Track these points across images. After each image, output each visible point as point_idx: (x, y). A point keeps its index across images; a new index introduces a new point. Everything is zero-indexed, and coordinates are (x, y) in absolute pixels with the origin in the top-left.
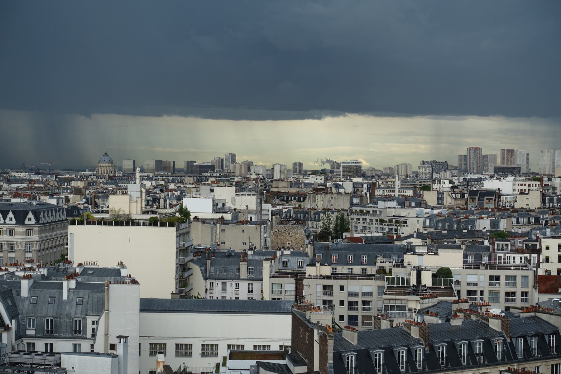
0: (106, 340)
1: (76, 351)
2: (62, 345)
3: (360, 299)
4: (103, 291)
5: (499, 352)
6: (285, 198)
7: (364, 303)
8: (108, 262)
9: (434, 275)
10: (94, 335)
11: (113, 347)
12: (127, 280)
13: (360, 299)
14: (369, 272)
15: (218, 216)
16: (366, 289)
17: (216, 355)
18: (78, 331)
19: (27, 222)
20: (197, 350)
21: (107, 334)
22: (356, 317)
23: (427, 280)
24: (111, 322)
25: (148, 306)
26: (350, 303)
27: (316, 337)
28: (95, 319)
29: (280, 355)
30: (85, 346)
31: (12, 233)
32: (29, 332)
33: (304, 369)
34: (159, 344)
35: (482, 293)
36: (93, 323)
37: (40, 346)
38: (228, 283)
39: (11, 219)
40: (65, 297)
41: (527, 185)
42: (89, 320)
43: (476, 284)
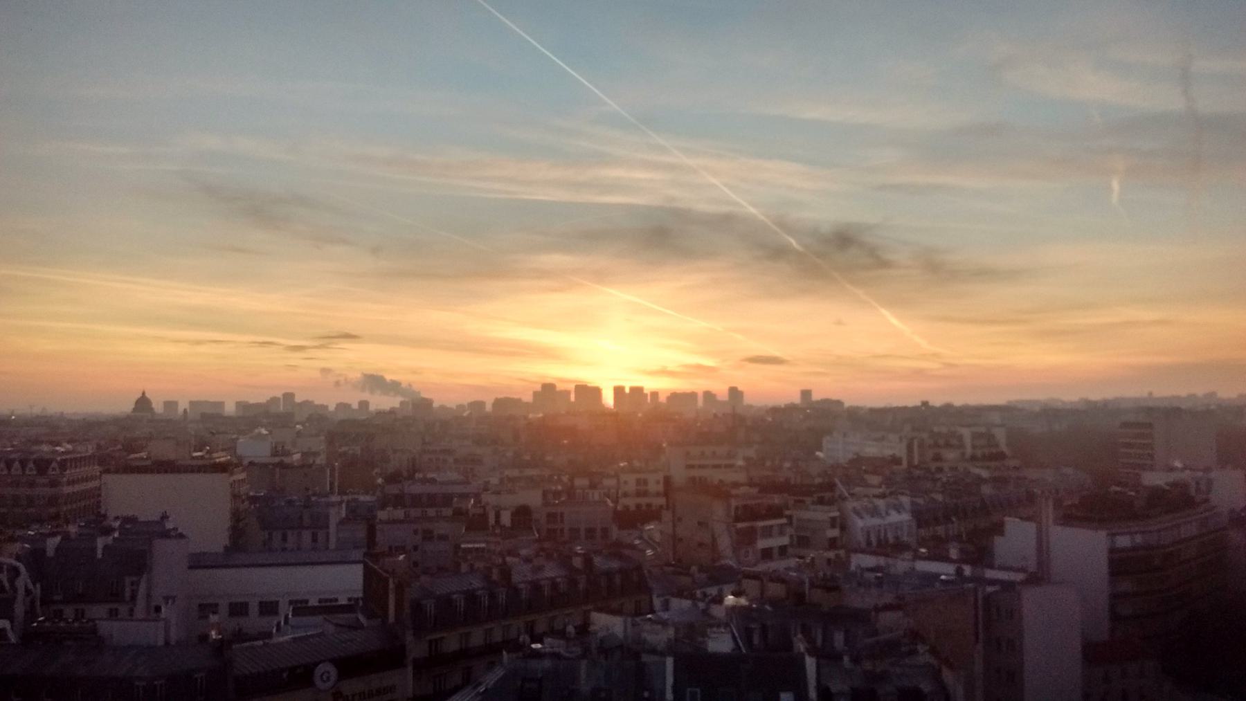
1: (113, 614)
2: (97, 611)
5: (487, 542)
8: (148, 513)
9: (512, 514)
10: (133, 597)
11: (158, 609)
12: (173, 533)
14: (444, 514)
15: (277, 460)
18: (115, 595)
19: (50, 472)
20: (254, 609)
21: (149, 596)
23: (506, 519)
25: (198, 562)
27: (391, 586)
28: (135, 579)
29: (349, 608)
30: (123, 609)
31: (32, 485)
32: (56, 598)
36: (132, 584)
37: (69, 612)
38: (289, 533)
39: (31, 470)
40: (99, 556)
42: (128, 580)
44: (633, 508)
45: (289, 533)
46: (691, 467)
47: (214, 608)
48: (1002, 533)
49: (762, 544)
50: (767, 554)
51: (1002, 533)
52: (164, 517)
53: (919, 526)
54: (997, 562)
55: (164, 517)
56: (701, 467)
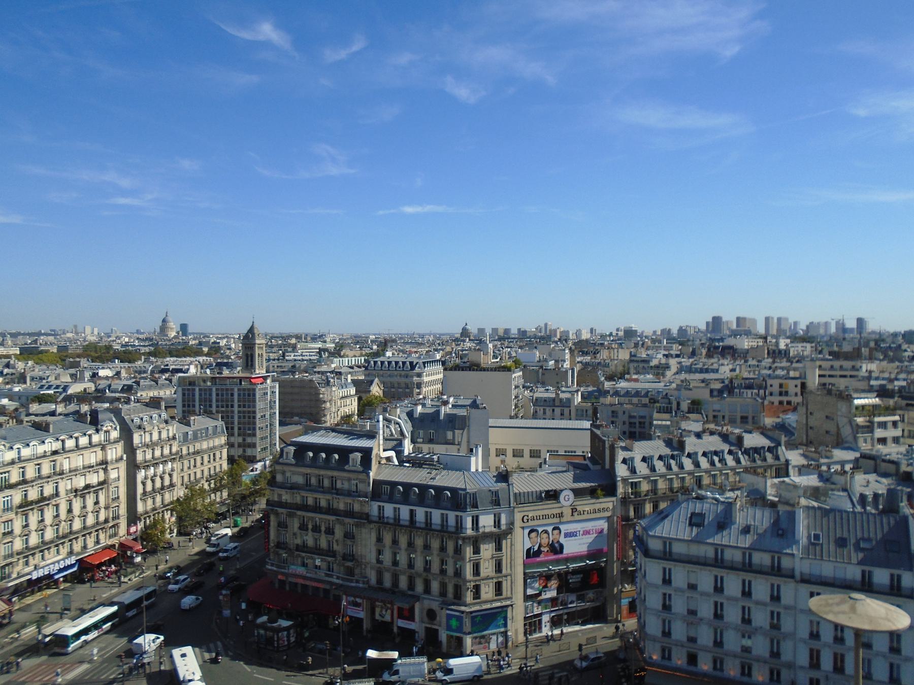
0: (468, 445)
3: (637, 421)
4: (91, 423)
6: (648, 508)
7: (640, 423)
13: (637, 421)
16: (642, 414)
17: (540, 457)
20: (527, 453)
22: (635, 433)
24: (472, 434)
26: (630, 423)
33: (598, 467)
34: (402, 484)
35: (723, 417)
38: (547, 409)
41: (339, 532)
43: (719, 411)
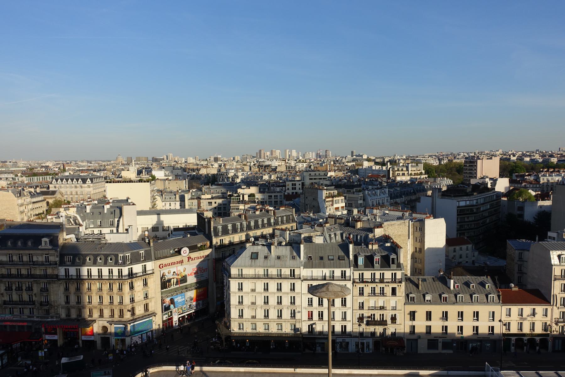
1: (112, 232)
38: (172, 203)
40: (105, 212)
44: (291, 194)
45: (172, 203)
46: (312, 179)
47: (418, 162)
48: (419, 202)
49: (336, 206)
50: (337, 209)
51: (419, 202)
52: (128, 198)
53: (391, 199)
54: (232, 276)
55: (128, 198)
56: (315, 179)
